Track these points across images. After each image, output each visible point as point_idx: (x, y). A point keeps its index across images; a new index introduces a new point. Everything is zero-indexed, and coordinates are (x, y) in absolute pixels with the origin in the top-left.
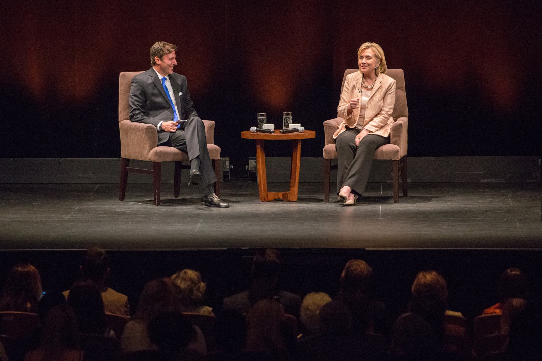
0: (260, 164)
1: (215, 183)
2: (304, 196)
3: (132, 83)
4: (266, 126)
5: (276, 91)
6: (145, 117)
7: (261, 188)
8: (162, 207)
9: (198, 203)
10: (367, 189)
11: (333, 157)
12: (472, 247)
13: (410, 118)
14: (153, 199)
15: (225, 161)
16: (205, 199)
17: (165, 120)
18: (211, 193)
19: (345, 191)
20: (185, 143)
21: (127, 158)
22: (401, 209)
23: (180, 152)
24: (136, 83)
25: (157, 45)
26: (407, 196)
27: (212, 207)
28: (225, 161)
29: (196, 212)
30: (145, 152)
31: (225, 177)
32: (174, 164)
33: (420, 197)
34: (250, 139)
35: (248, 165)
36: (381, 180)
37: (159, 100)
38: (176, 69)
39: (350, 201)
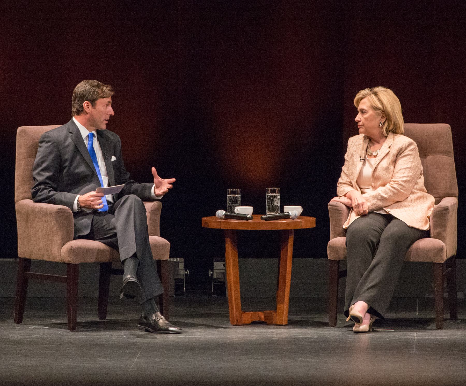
0: (230, 268)
1: (161, 296)
2: (298, 318)
3: (41, 142)
4: (239, 210)
5: (255, 157)
9: (135, 327)
10: (391, 308)
11: (342, 258)
13: (459, 199)
14: (66, 321)
15: (177, 263)
16: (145, 321)
19: (358, 308)
20: (115, 235)
21: (27, 257)
23: (108, 248)
25: (82, 87)
26: (456, 319)
27: (156, 333)
28: (177, 263)
29: (132, 341)
30: (55, 249)
31: (178, 288)
35: (212, 270)
37: (82, 169)
38: (112, 123)
39: (364, 326)
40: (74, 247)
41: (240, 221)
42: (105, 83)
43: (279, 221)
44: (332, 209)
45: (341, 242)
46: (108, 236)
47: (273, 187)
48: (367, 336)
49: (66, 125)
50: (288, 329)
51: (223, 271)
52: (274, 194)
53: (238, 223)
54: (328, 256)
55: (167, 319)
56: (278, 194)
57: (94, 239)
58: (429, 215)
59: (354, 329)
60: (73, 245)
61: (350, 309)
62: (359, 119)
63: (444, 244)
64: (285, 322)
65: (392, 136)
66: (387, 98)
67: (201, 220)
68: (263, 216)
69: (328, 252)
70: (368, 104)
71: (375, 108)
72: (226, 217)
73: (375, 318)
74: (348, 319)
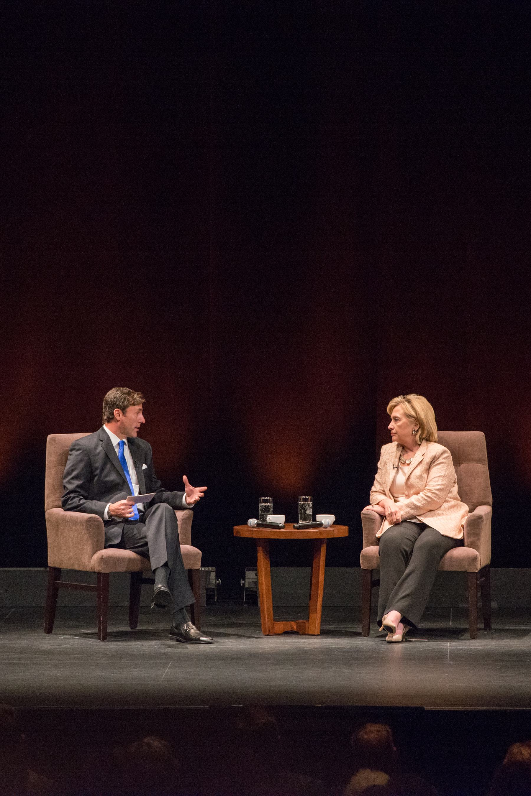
0: (261, 577)
1: (192, 605)
2: (331, 627)
3: (71, 450)
4: (271, 518)
5: (287, 466)
8: (110, 643)
9: (166, 637)
10: (425, 617)
11: (375, 567)
12: (516, 706)
14: (96, 631)
15: (209, 572)
16: (176, 631)
19: (392, 618)
20: (146, 544)
22: (481, 648)
25: (112, 394)
26: (490, 629)
27: (187, 643)
28: (209, 572)
30: (85, 558)
31: (209, 597)
32: (129, 576)
33: (509, 630)
34: (247, 538)
35: (244, 580)
36: (447, 600)
37: (113, 477)
38: (142, 430)
39: (397, 636)
40: (105, 556)
43: (311, 530)
44: (365, 518)
45: (374, 551)
46: (139, 544)
47: (305, 496)
48: (400, 645)
49: (97, 433)
50: (320, 638)
51: (255, 580)
53: (270, 531)
55: (198, 628)
57: (124, 548)
58: (463, 523)
59: (387, 639)
60: (103, 554)
62: (392, 427)
63: (478, 553)
65: (426, 444)
66: (420, 405)
67: (233, 529)
68: (296, 525)
69: (361, 561)
70: (402, 411)
71: (409, 416)
72: (258, 525)
73: (409, 627)
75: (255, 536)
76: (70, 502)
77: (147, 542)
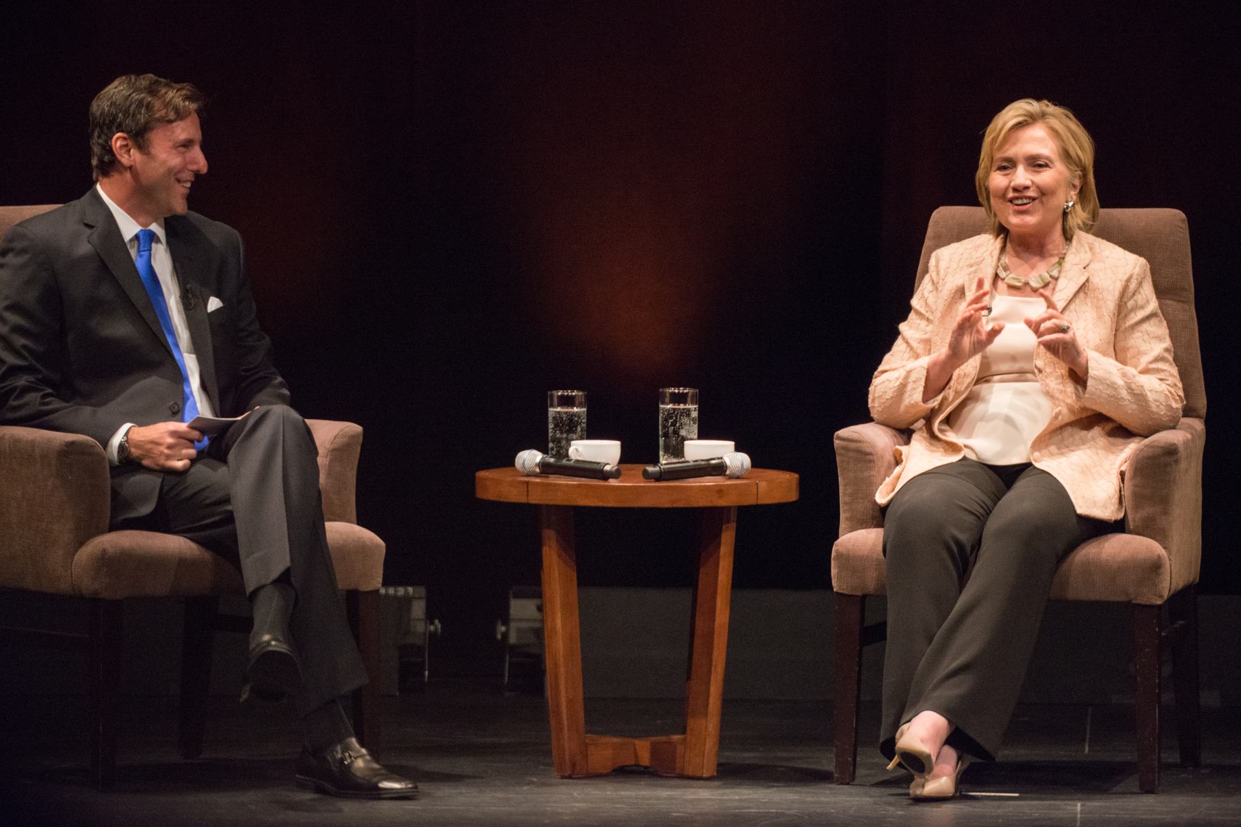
0: (554, 614)
1: (357, 694)
2: (748, 757)
4: (583, 449)
5: (632, 297)
6: (56, 404)
7: (559, 722)
17: (143, 419)
18: (341, 739)
19: (922, 731)
20: (230, 518)
23: (207, 555)
24: (23, 251)
25: (117, 91)
28: (407, 601)
35: (506, 622)
37: (120, 329)
39: (941, 782)
40: (111, 551)
41: (584, 481)
42: (175, 77)
44: (844, 448)
45: (870, 542)
47: (678, 386)
48: (947, 809)
49: (77, 205)
50: (719, 787)
51: (537, 625)
52: (682, 406)
53: (579, 486)
54: (834, 583)
55: (375, 755)
56: (692, 407)
58: (1123, 468)
59: (915, 790)
60: (107, 546)
61: (897, 735)
63: (1163, 552)
64: (709, 769)
67: (474, 477)
68: (650, 469)
72: (545, 469)
73: (970, 759)
74: (890, 766)
75: (534, 499)
76: (14, 403)
77: (231, 512)
